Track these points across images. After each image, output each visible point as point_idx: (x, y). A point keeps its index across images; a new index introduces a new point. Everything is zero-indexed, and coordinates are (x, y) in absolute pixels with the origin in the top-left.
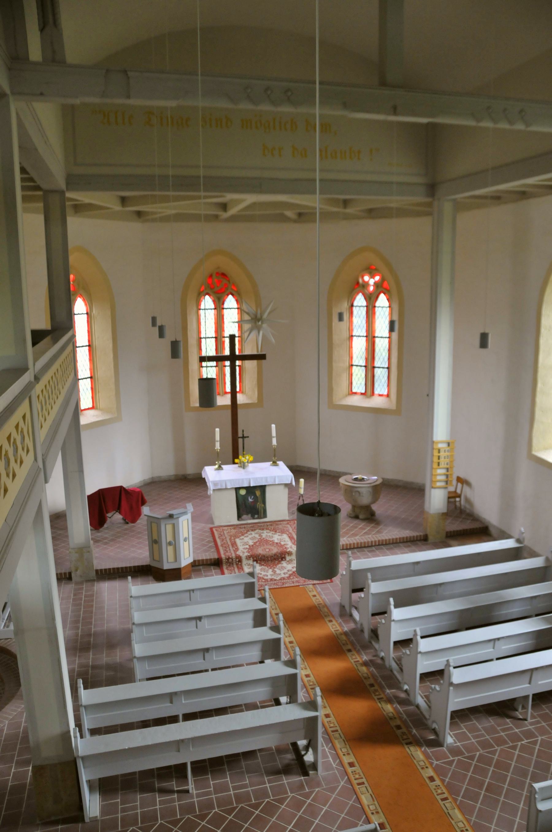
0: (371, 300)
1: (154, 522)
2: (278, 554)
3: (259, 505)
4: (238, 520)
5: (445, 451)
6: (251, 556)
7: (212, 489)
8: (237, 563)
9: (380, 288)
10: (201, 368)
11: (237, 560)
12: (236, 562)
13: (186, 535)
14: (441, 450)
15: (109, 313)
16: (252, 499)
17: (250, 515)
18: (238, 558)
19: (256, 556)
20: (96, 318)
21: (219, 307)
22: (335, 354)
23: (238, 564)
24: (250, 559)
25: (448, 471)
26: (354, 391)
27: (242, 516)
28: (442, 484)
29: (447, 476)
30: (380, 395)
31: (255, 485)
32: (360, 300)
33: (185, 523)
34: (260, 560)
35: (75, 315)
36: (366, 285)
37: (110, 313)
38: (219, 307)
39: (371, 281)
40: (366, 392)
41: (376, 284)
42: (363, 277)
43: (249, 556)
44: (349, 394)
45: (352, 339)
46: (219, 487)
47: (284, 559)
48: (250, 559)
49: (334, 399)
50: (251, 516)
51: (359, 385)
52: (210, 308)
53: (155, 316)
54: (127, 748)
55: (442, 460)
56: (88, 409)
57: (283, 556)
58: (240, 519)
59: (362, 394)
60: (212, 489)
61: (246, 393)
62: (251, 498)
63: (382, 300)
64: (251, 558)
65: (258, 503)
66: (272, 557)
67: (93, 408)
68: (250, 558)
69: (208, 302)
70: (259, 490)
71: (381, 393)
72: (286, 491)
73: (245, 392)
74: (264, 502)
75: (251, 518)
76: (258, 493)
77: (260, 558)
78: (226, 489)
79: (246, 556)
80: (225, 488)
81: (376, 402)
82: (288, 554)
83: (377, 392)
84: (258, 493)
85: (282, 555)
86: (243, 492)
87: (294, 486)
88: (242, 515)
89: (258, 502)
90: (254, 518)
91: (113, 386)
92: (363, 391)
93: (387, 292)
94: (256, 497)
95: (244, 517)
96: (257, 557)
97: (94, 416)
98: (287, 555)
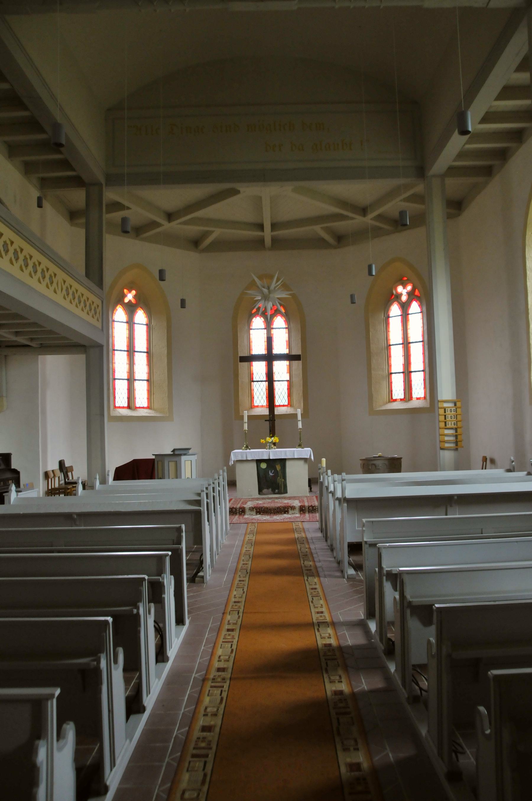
0: (405, 307)
1: (160, 461)
2: (281, 508)
3: (280, 480)
4: (259, 494)
5: (451, 411)
6: (254, 507)
7: (233, 459)
8: (241, 513)
9: (412, 296)
10: (252, 383)
11: (241, 510)
12: (240, 512)
13: (188, 475)
14: (446, 409)
15: (165, 324)
16: (272, 474)
17: (270, 489)
18: (242, 509)
19: (259, 508)
20: (154, 329)
21: (269, 326)
22: (374, 362)
23: (241, 514)
24: (253, 511)
25: (456, 432)
26: (394, 398)
27: (263, 490)
28: (452, 445)
29: (456, 436)
30: (418, 399)
31: (274, 458)
32: (395, 310)
33: (188, 464)
34: (263, 511)
35: (135, 325)
36: (399, 296)
37: (166, 324)
38: (269, 326)
39: (403, 291)
40: (404, 398)
41: (409, 294)
42: (396, 289)
43: (252, 507)
44: (389, 402)
45: (390, 349)
46: (240, 458)
47: (287, 513)
48: (253, 511)
49: (374, 405)
50: (272, 490)
51: (398, 392)
52: (260, 328)
53: (164, 268)
54: (21, 513)
55: (448, 419)
56: (143, 408)
57: (286, 509)
58: (261, 493)
59: (401, 400)
60: (233, 459)
61: (294, 406)
62: (271, 473)
63: (415, 307)
64: (254, 510)
65: (279, 478)
66: (275, 509)
67: (148, 408)
68: (253, 509)
69: (258, 322)
70: (279, 465)
71: (418, 397)
72: (306, 467)
73: (293, 405)
74: (284, 477)
75: (272, 492)
76: (278, 467)
77: (262, 509)
78: (247, 461)
79: (250, 507)
80: (245, 459)
81: (414, 404)
82: (291, 508)
83: (415, 395)
84: (278, 467)
85: (285, 509)
86: (264, 466)
87: (313, 461)
88: (263, 489)
89: (278, 476)
90: (275, 493)
91: (166, 389)
92: (402, 397)
93: (418, 299)
94: (276, 472)
95: (265, 491)
96: (260, 509)
97: (146, 413)
98: (290, 509)
